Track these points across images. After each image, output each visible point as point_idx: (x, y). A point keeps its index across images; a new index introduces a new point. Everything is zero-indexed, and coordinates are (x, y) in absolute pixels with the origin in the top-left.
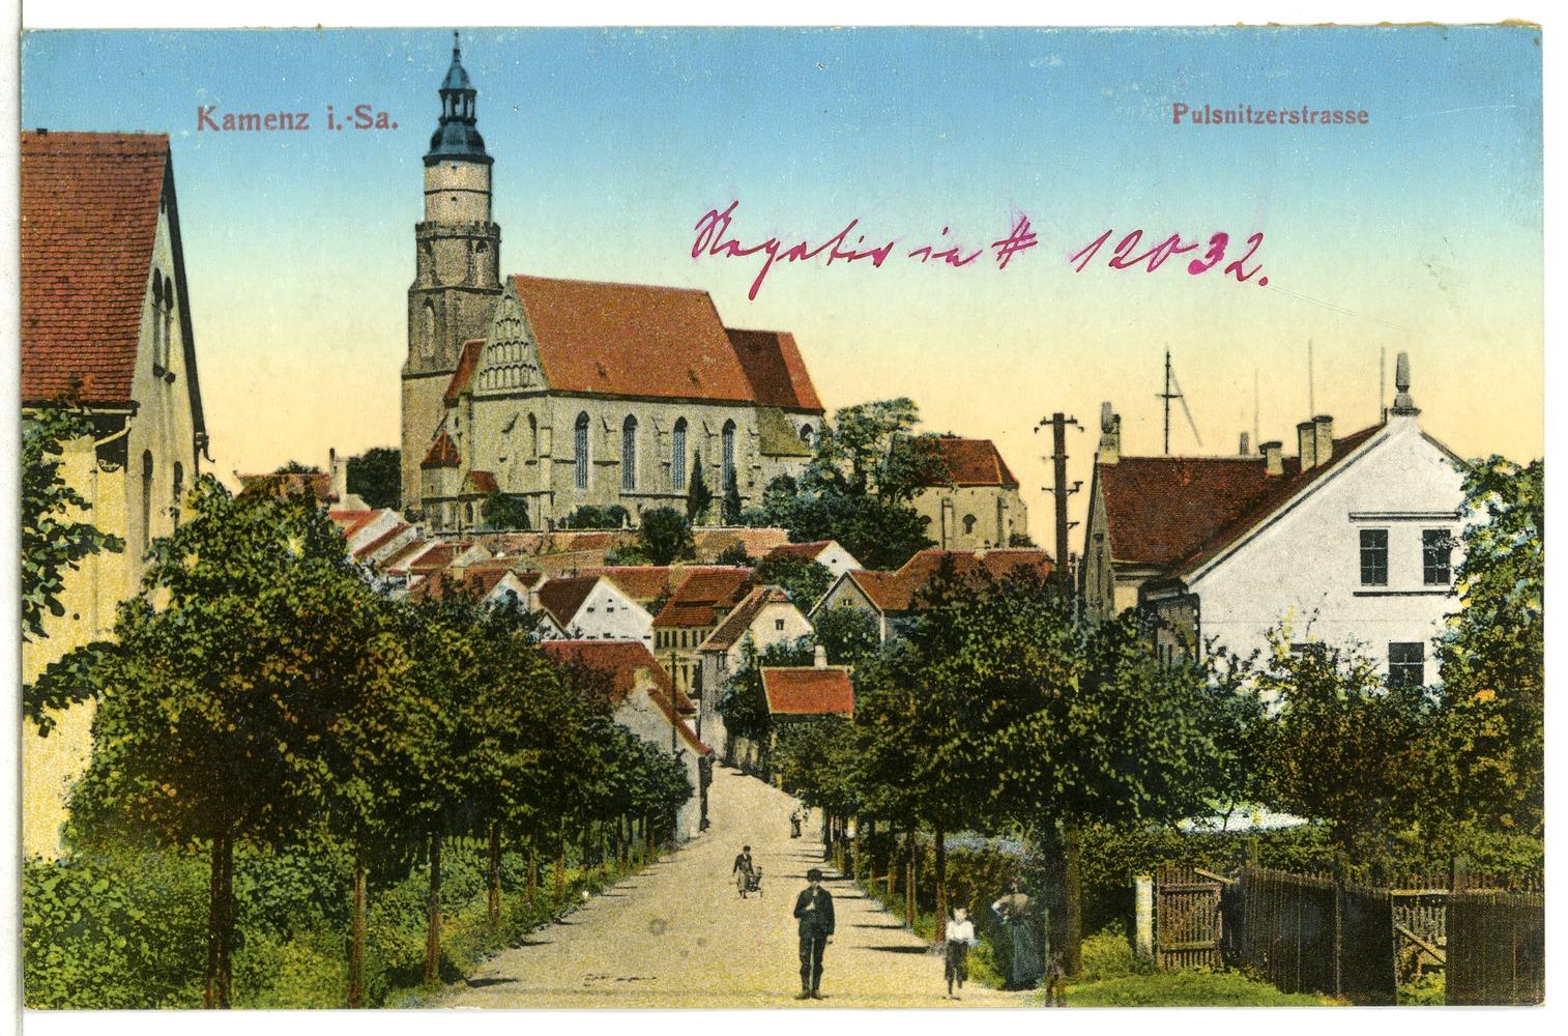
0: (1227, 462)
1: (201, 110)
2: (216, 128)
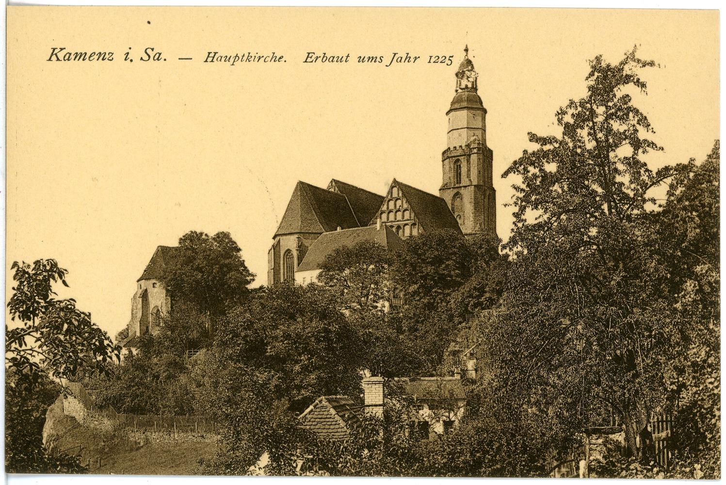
0: (323, 190)
2: (58, 59)
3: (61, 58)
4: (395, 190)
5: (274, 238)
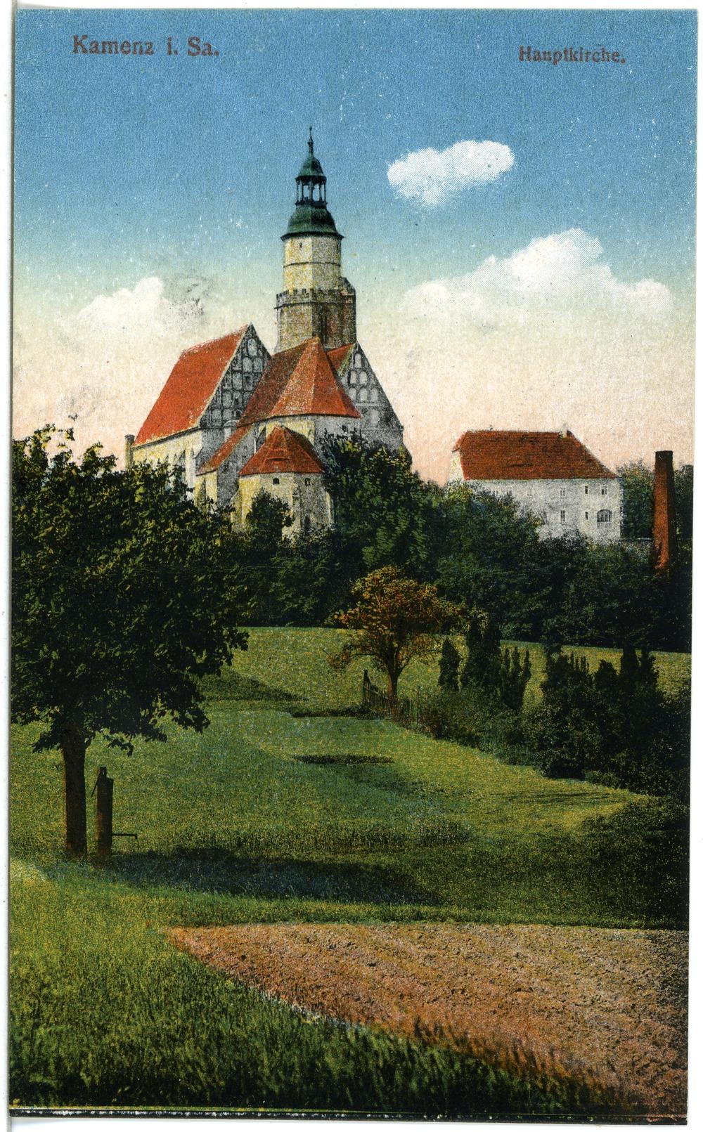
1: (76, 38)
3: (88, 47)
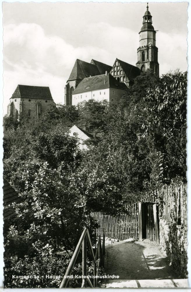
0: (89, 64)
4: (117, 63)
5: (67, 83)
